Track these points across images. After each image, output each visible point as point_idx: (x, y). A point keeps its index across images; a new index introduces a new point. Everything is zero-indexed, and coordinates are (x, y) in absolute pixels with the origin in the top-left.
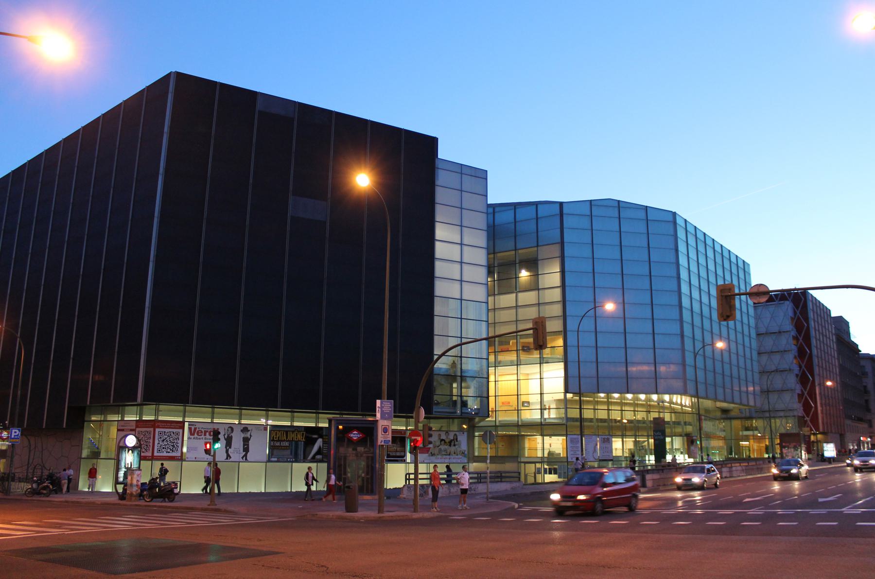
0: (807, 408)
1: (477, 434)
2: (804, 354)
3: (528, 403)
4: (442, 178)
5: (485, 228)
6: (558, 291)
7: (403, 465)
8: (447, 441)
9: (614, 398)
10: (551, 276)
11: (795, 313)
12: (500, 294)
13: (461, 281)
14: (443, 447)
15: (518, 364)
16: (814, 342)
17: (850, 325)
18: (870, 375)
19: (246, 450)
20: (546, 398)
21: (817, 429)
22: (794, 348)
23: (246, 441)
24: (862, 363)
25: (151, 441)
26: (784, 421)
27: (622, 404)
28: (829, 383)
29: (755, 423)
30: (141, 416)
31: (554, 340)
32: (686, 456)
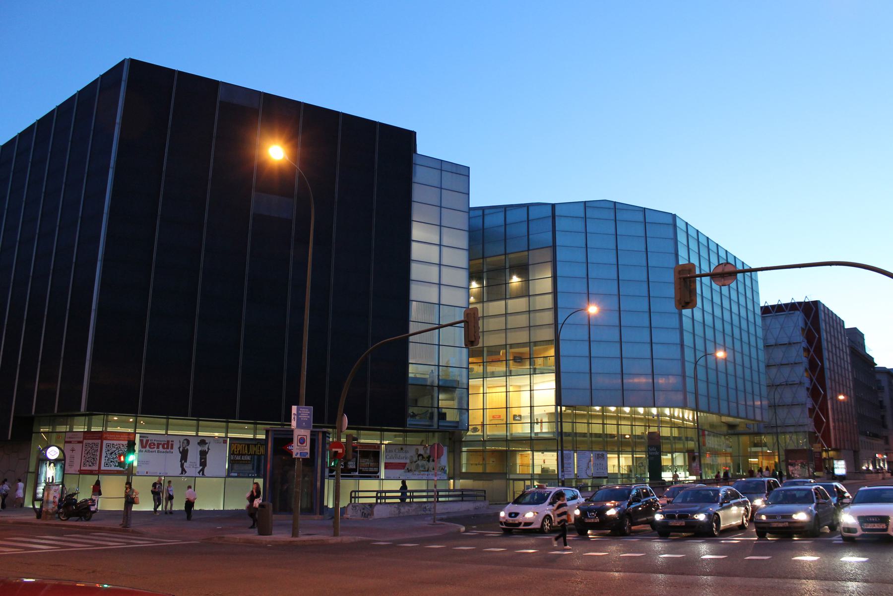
0: (818, 423)
1: (464, 449)
2: (815, 367)
3: (520, 416)
4: (420, 174)
5: (466, 228)
6: (550, 297)
7: (377, 481)
8: (425, 456)
9: (610, 412)
10: (543, 282)
11: (806, 324)
12: (488, 301)
13: (440, 284)
14: (420, 463)
15: (508, 374)
16: (825, 354)
17: (865, 337)
18: (886, 389)
19: (203, 464)
20: (537, 411)
21: (829, 445)
22: (805, 361)
23: (203, 454)
24: (878, 376)
25: (98, 454)
26: (794, 437)
27: (618, 418)
28: (841, 397)
29: (764, 439)
30: (89, 427)
31: (546, 350)
32: (688, 473)
